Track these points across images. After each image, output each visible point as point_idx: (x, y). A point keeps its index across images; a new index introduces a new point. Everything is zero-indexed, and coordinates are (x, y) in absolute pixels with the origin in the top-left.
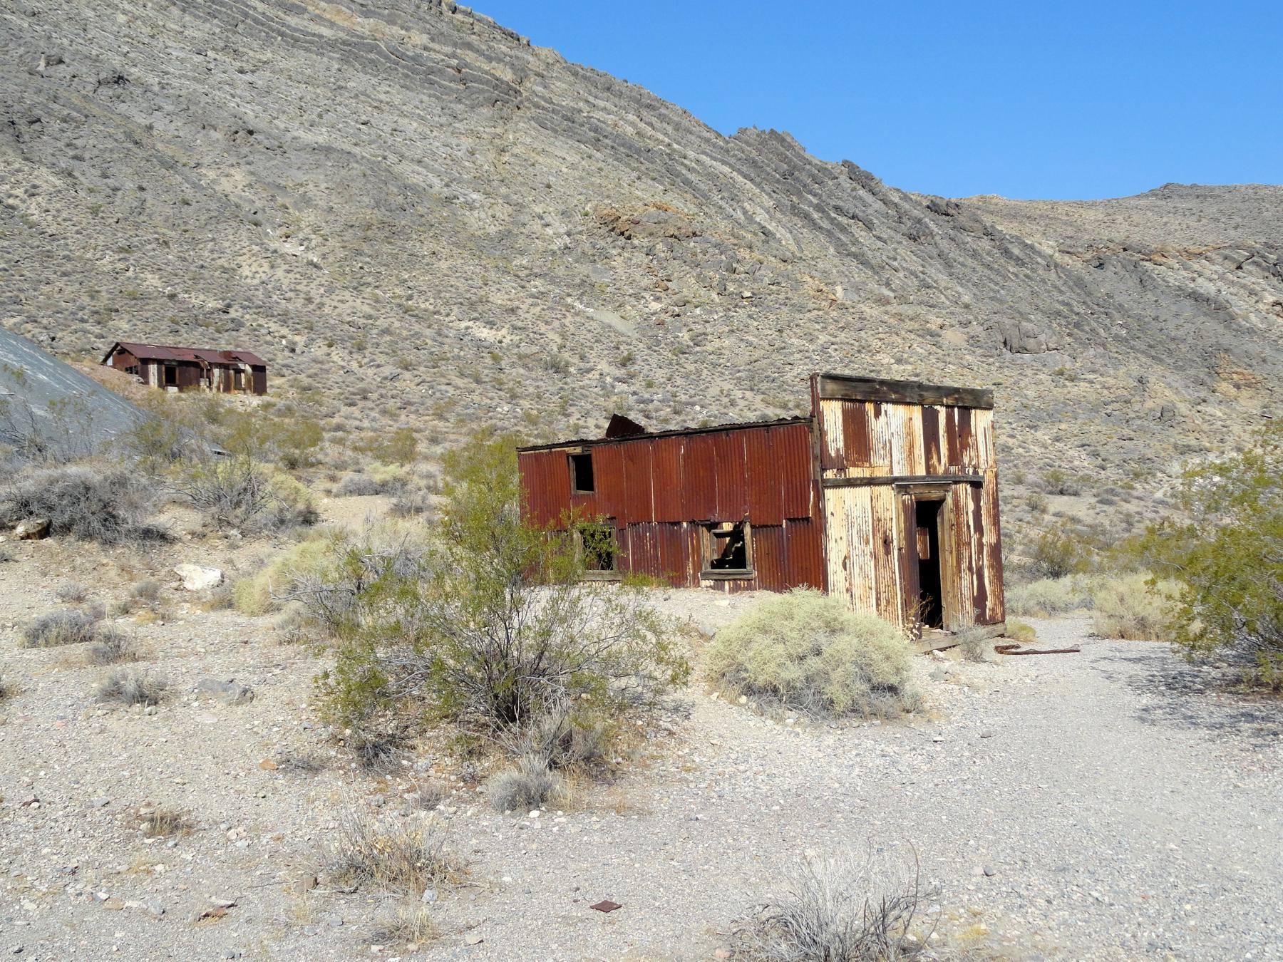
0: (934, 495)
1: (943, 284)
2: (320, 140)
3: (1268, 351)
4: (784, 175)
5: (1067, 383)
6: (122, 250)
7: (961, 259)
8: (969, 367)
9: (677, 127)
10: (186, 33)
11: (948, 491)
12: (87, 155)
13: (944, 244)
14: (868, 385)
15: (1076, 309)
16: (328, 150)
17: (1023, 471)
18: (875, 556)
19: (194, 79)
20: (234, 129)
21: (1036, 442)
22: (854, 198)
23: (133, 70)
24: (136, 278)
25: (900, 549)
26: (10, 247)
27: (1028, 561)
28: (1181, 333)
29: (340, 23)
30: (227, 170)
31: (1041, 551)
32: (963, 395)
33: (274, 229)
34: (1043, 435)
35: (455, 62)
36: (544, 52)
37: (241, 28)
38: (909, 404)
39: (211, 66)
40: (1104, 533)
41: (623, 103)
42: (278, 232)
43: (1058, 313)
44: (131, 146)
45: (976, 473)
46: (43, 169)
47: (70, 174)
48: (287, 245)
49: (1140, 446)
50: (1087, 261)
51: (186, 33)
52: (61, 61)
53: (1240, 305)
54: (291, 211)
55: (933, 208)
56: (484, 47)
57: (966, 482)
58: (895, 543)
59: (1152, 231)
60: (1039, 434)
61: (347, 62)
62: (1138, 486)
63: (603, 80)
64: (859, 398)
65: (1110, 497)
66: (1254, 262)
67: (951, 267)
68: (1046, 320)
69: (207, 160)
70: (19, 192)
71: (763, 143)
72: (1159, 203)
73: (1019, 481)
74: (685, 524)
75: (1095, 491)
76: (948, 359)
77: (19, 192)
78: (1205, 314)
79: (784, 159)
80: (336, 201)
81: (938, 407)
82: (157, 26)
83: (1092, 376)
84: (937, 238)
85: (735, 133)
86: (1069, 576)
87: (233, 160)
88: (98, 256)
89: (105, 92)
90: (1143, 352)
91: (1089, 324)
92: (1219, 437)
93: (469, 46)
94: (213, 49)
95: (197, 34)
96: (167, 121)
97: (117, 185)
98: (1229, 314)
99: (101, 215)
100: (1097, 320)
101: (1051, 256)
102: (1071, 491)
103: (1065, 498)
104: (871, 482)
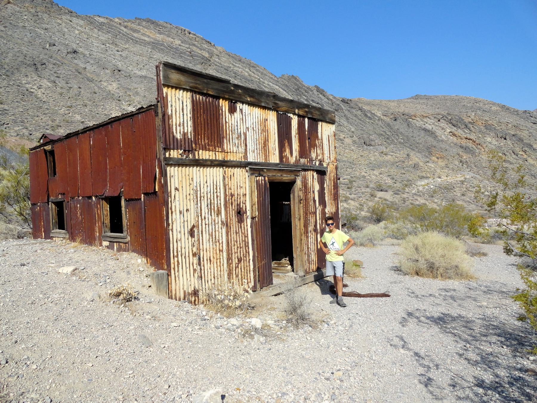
0: (286, 178)
1: (346, 125)
2: (143, 74)
3: (447, 147)
4: (296, 90)
5: (384, 156)
6: (68, 107)
7: (352, 117)
8: (353, 150)
9: (262, 73)
10: (99, 38)
11: (298, 176)
12: (61, 76)
13: (346, 112)
14: (223, 84)
15: (387, 133)
16: (145, 77)
17: (369, 183)
18: (227, 225)
19: (101, 53)
20: (114, 69)
21: (374, 174)
22: (318, 97)
23: (80, 49)
24: (72, 116)
25: (253, 218)
26: (26, 104)
27: (368, 214)
28: (420, 141)
29: (151, 36)
30: (111, 83)
31: (373, 211)
32: (312, 110)
33: (125, 102)
34: (376, 172)
35: (189, 50)
36: (219, 48)
37: (118, 37)
38: (264, 108)
39: (107, 49)
40: (396, 204)
41: (244, 65)
42: (127, 103)
43: (382, 135)
44: (77, 74)
45: (321, 164)
46: (45, 80)
47: (55, 82)
48: (129, 108)
49: (408, 176)
50: (391, 118)
51: (99, 38)
52: (54, 45)
53: (439, 132)
54: (132, 97)
55: (343, 101)
56: (199, 46)
57: (313, 170)
58: (249, 213)
59: (412, 109)
60: (375, 172)
61: (154, 49)
62: (406, 189)
63: (238, 58)
64: (211, 93)
65: (398, 192)
66: (444, 119)
67: (348, 120)
68: (378, 137)
69: (104, 79)
70: (35, 87)
71: (290, 79)
72: (414, 101)
73: (367, 187)
74: (94, 198)
75: (393, 190)
76: (346, 148)
77: (35, 87)
78: (428, 135)
79: (296, 85)
80: (147, 94)
81: (291, 115)
82: (90, 35)
83: (392, 154)
84: (344, 110)
85: (281, 76)
86: (384, 222)
87: (113, 80)
88: (60, 109)
89: (70, 56)
90: (408, 147)
91: (391, 138)
92: (433, 173)
93: (194, 45)
94: (108, 43)
95: (103, 38)
96: (91, 66)
97: (71, 86)
98: (435, 135)
99: (63, 95)
100: (394, 137)
101: (380, 117)
102: (385, 190)
103: (383, 192)
104: (223, 164)
